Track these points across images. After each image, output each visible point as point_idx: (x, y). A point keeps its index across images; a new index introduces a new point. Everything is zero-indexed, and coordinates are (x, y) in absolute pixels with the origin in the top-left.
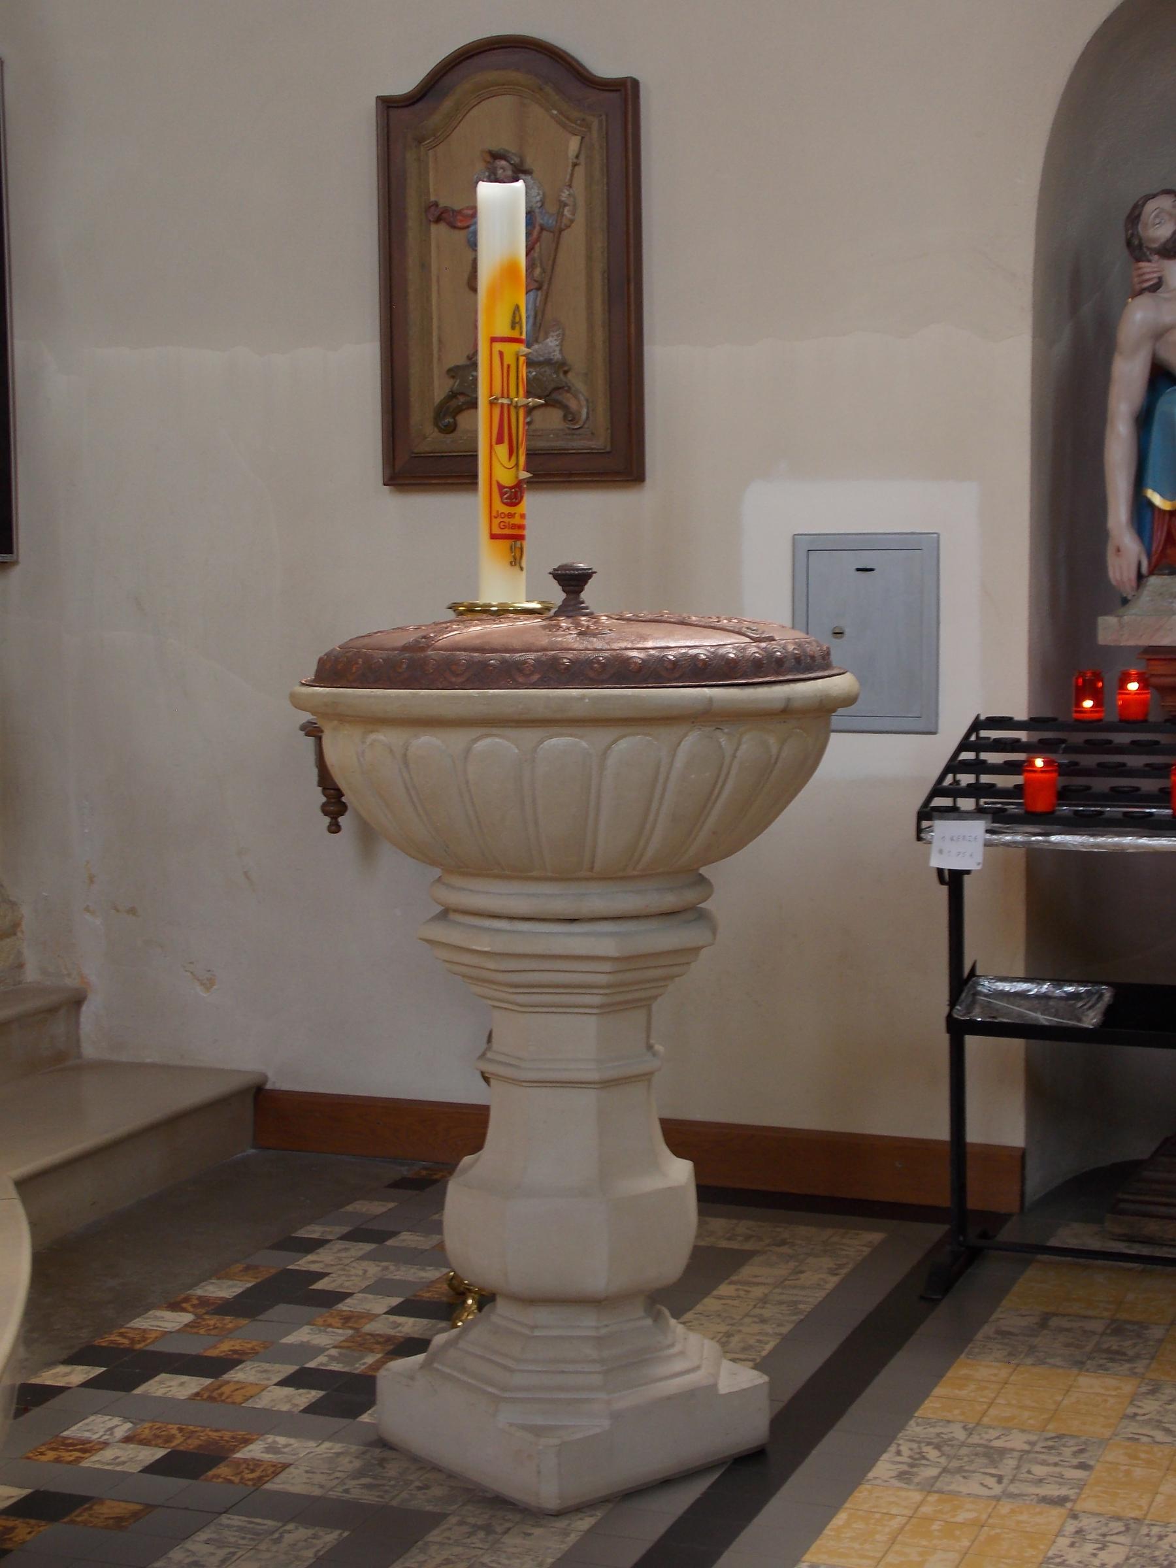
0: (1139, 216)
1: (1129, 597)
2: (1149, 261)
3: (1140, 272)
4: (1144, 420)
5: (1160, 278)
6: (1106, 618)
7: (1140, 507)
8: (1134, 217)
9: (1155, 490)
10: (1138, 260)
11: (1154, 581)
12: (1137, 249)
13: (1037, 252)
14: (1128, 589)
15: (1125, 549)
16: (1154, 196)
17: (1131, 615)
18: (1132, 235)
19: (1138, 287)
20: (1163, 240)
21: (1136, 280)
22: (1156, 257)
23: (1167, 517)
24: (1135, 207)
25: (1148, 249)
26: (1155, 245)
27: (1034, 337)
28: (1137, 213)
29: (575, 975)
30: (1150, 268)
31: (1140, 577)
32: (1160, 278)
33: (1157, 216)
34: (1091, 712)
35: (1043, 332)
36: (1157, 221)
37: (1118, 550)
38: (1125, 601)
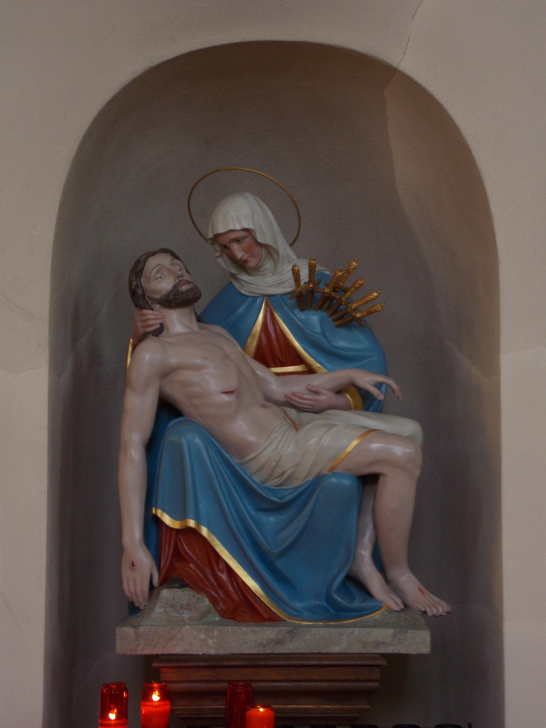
0: (142, 271)
1: (142, 607)
2: (152, 309)
3: (144, 318)
4: (152, 447)
5: (162, 325)
6: (123, 629)
7: (152, 523)
8: (138, 269)
9: (164, 510)
10: (142, 308)
11: (165, 593)
12: (139, 298)
13: (52, 296)
14: (141, 601)
15: (140, 564)
16: (154, 254)
17: (146, 625)
18: (137, 286)
19: (141, 331)
20: (164, 292)
21: (140, 324)
22: (158, 306)
23: (174, 533)
24: (138, 262)
25: (149, 297)
26: (157, 296)
27: (50, 370)
28: (140, 267)
29: (309, 684)
30: (153, 316)
31: (152, 587)
32: (162, 325)
33: (158, 272)
34: (158, 706)
35: (56, 367)
36: (159, 276)
37: (133, 565)
38: (133, 609)
